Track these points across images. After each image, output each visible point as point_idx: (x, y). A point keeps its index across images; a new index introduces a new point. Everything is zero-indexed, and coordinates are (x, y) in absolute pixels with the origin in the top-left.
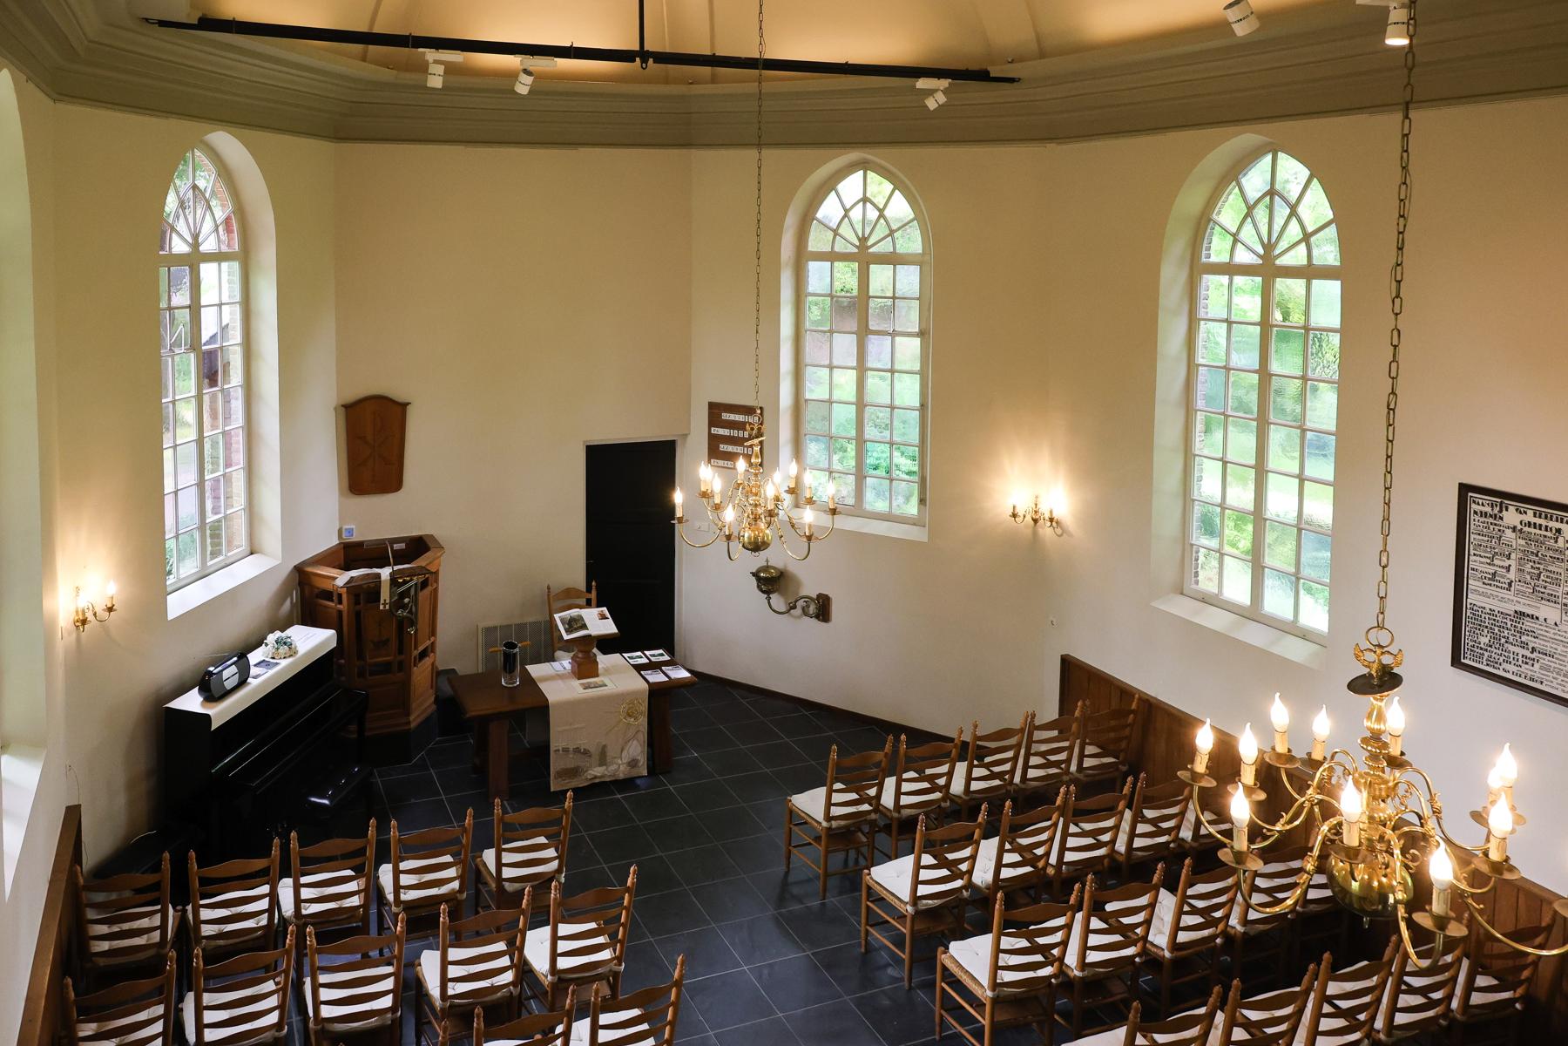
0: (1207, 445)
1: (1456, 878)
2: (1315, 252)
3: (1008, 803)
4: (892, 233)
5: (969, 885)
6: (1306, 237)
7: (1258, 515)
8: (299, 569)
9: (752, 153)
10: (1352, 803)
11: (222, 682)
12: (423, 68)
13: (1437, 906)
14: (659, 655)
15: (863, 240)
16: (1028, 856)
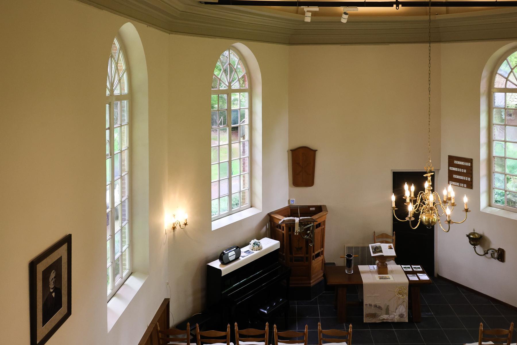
8: (269, 215)
9: (428, 45)
11: (228, 257)
12: (303, 13)
14: (418, 268)
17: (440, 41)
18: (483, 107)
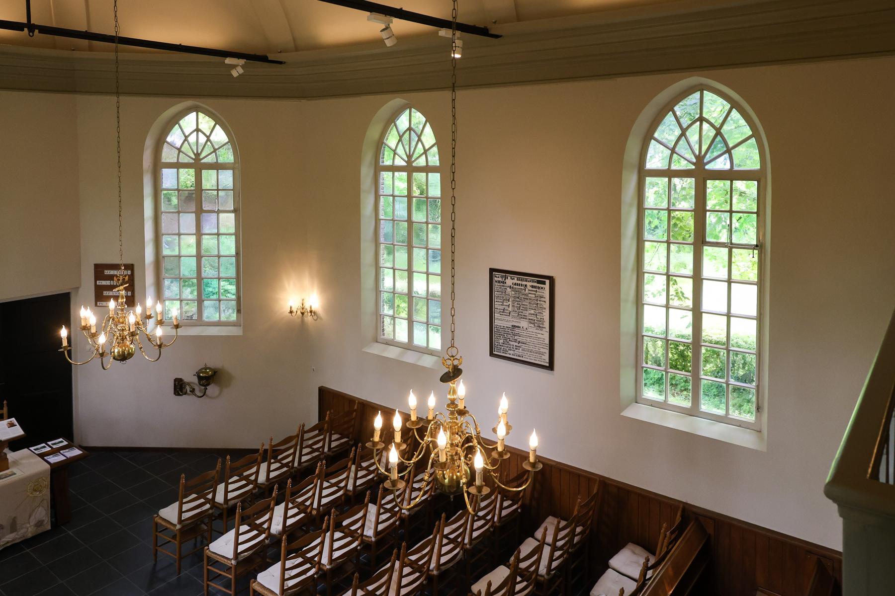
0: (385, 260)
1: (486, 464)
2: (429, 159)
3: (289, 481)
4: (215, 151)
5: (270, 536)
6: (426, 152)
7: (410, 295)
9: (114, 99)
10: (443, 439)
13: (478, 482)
14: (61, 442)
15: (197, 155)
16: (302, 507)
17: (75, 92)
18: (148, 190)
